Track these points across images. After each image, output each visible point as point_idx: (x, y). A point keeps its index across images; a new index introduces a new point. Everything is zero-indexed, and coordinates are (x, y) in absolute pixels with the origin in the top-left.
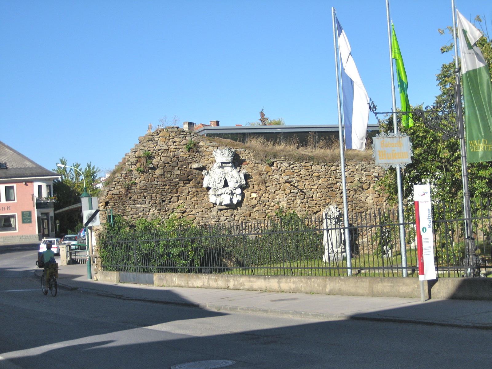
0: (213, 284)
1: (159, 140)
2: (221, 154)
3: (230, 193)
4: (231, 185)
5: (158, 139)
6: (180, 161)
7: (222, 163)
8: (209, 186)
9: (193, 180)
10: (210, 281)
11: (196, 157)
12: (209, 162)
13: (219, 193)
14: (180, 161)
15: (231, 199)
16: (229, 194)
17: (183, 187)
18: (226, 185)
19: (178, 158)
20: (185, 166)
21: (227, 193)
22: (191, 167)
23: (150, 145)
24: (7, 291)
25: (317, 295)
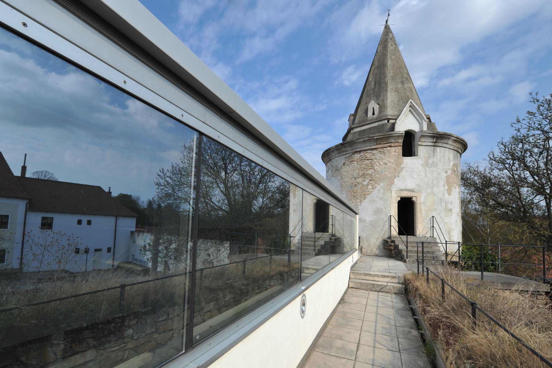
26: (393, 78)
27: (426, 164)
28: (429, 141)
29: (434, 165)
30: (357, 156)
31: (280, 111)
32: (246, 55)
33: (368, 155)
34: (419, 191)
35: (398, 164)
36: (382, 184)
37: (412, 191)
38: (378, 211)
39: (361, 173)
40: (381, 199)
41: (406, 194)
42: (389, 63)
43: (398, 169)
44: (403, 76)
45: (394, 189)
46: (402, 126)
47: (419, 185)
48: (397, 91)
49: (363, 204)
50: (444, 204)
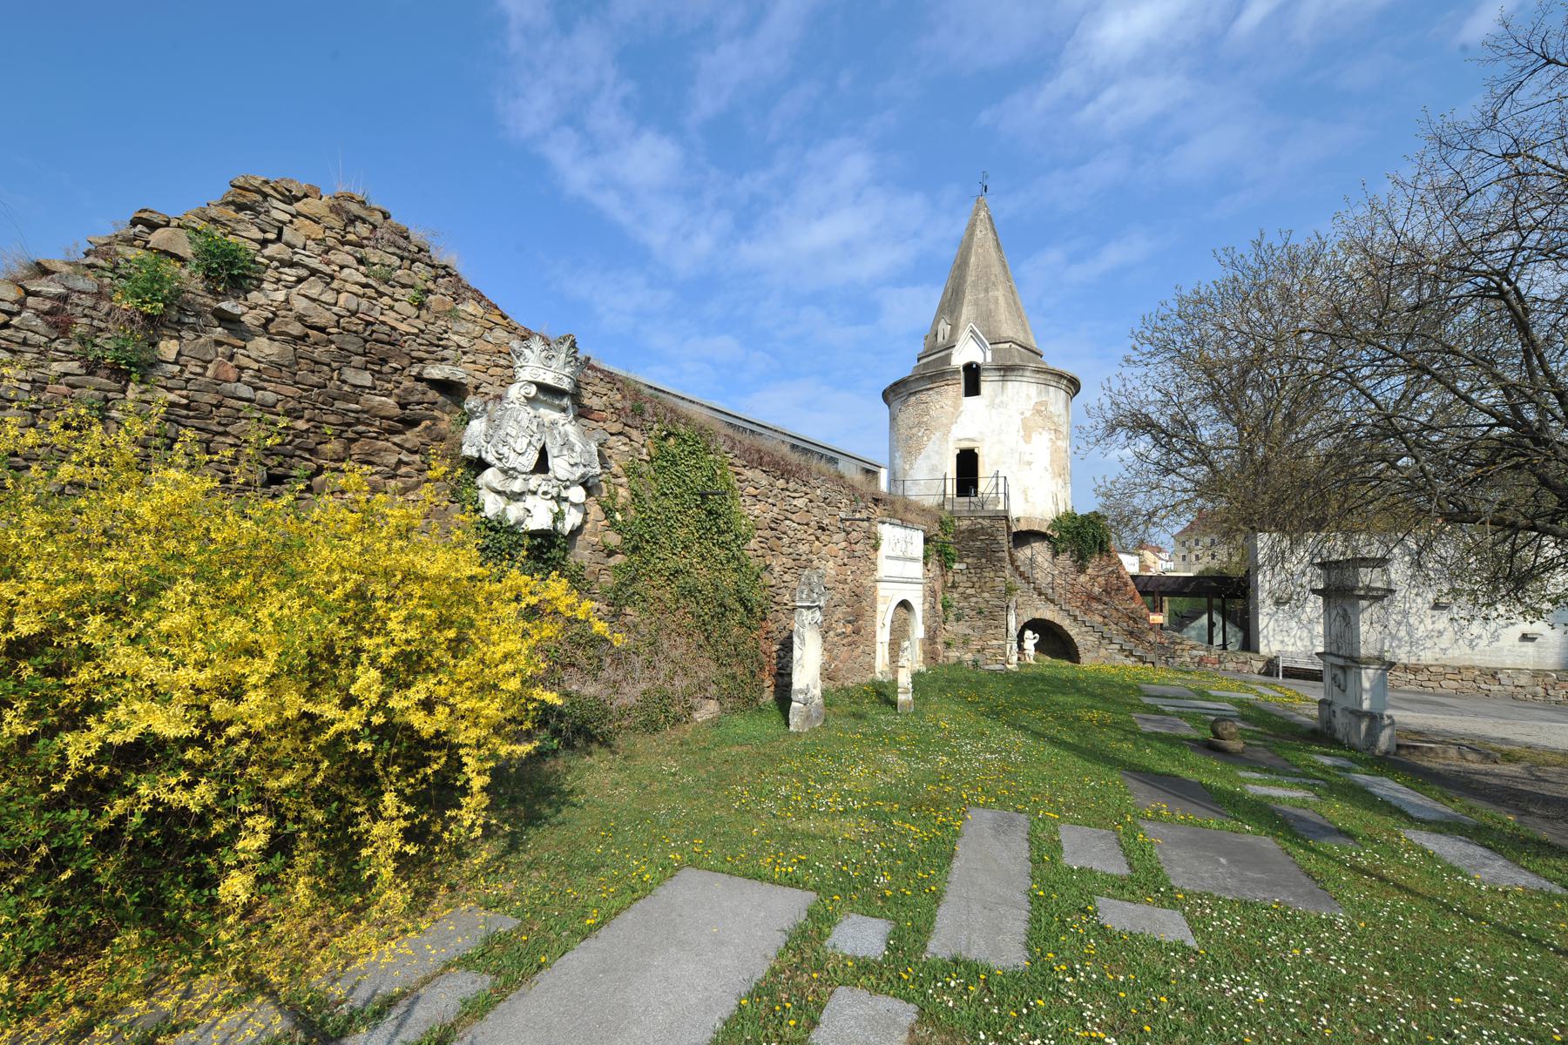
0: (949, 483)
1: (291, 222)
2: (544, 354)
3: (555, 494)
4: (559, 466)
5: (288, 217)
6: (377, 341)
7: (543, 388)
8: (484, 456)
9: (424, 424)
10: (1144, 443)
11: (445, 347)
12: (490, 380)
13: (517, 486)
14: (377, 341)
15: (558, 517)
16: (552, 498)
17: (377, 438)
18: (542, 466)
19: (372, 324)
20: (394, 365)
21: (545, 493)
22: (419, 373)
23: (238, 227)
24: (1259, 729)
25: (707, 872)
26: (975, 284)
27: (992, 405)
28: (995, 376)
29: (1002, 405)
30: (913, 399)
31: (848, 249)
32: (705, 104)
33: (924, 396)
34: (983, 440)
35: (956, 406)
36: (937, 434)
37: (973, 440)
38: (933, 469)
39: (916, 420)
40: (937, 452)
41: (966, 445)
42: (973, 260)
43: (956, 413)
44: (989, 279)
45: (951, 438)
46: (959, 359)
47: (981, 433)
48: (976, 303)
49: (919, 461)
50: (1017, 456)
